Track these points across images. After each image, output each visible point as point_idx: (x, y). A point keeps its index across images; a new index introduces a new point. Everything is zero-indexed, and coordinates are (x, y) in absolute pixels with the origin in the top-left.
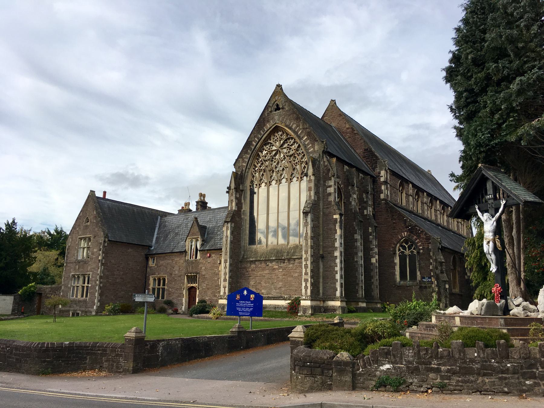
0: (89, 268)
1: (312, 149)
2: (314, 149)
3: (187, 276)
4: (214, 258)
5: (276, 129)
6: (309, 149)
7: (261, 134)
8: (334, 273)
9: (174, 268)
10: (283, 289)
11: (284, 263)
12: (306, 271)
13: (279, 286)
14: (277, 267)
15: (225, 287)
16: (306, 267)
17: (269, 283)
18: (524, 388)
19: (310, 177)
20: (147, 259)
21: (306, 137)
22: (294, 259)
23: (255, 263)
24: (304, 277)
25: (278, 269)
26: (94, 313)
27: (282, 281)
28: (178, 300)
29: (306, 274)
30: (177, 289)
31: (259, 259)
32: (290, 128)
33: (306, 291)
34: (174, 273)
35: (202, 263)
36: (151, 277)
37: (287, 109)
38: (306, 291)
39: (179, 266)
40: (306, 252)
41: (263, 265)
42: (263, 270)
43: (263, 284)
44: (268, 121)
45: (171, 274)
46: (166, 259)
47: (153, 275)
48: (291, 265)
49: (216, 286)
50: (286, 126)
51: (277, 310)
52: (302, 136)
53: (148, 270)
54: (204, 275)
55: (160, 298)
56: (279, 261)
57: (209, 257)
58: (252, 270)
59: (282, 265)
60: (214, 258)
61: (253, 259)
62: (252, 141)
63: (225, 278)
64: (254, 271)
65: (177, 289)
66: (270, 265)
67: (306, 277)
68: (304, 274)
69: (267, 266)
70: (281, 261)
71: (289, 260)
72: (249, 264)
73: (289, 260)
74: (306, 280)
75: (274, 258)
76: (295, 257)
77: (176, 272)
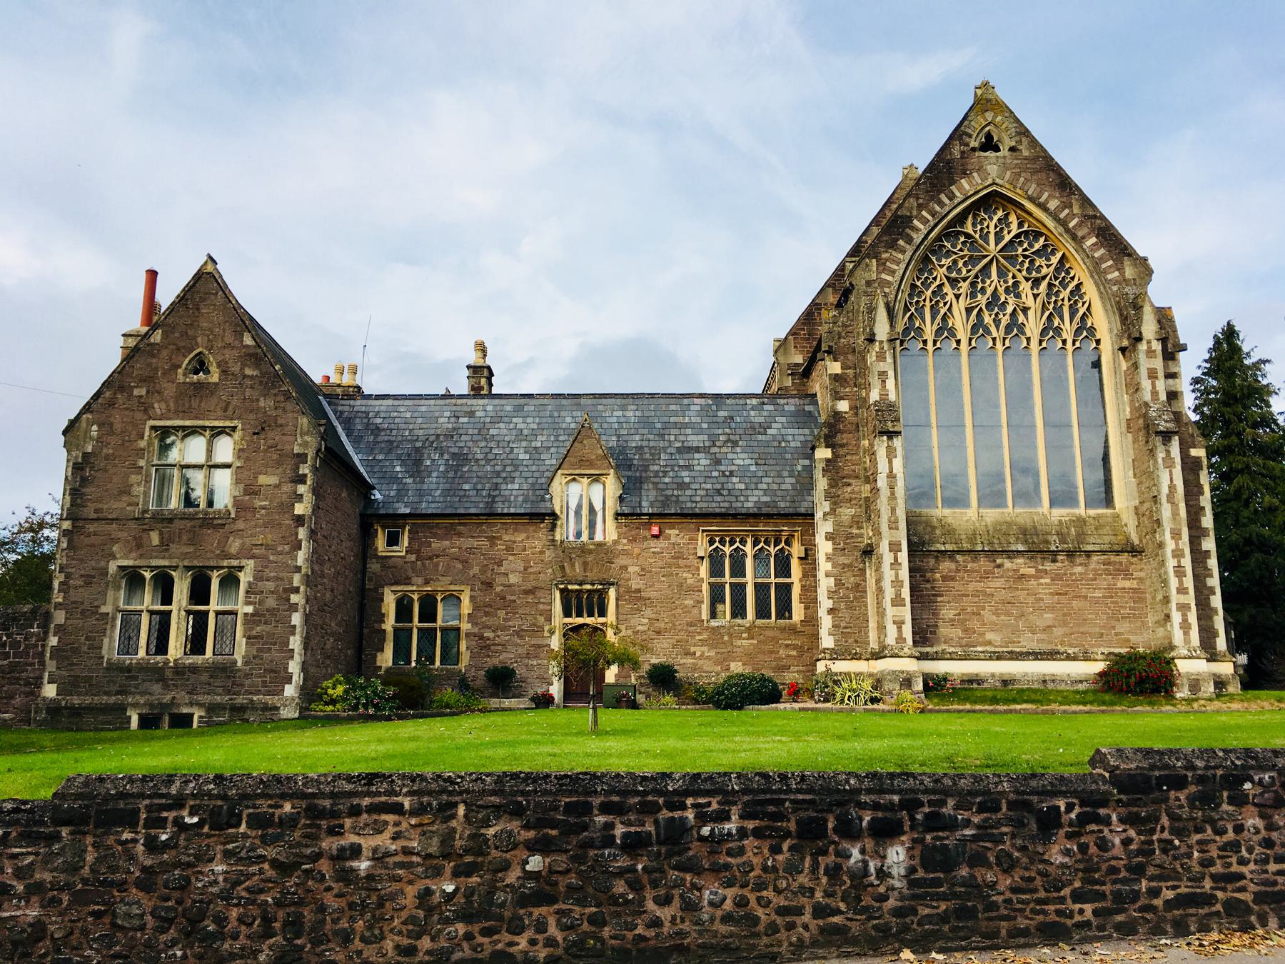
0: (235, 545)
1: (1117, 274)
2: (1122, 274)
3: (562, 591)
4: (673, 540)
5: (990, 201)
6: (1105, 272)
7: (942, 204)
8: (1206, 592)
9: (500, 564)
10: (1058, 632)
11: (1054, 561)
12: (1181, 583)
13: (1041, 624)
14: (1032, 571)
15: (899, 624)
16: (1179, 572)
17: (1008, 614)
18: (968, 832)
19: (1149, 342)
20: (366, 535)
21: (1094, 240)
22: (1089, 554)
23: (952, 558)
24: (1175, 598)
25: (1036, 577)
26: (289, 713)
27: (1051, 609)
28: (530, 669)
29: (1182, 590)
30: (519, 633)
31: (966, 546)
32: (1043, 207)
33: (1186, 634)
34: (500, 580)
35: (626, 553)
36: (387, 591)
37: (1026, 153)
38: (1186, 634)
39: (526, 560)
40: (1176, 535)
41: (983, 564)
42: (985, 577)
43: (987, 615)
44: (965, 173)
45: (489, 585)
46: (460, 535)
47: (397, 583)
48: (1079, 569)
49: (690, 624)
50: (1031, 199)
51: (1050, 686)
52: (1080, 234)
53: (374, 567)
54: (639, 591)
55: (438, 663)
56: (1039, 555)
57: (656, 537)
58: (944, 578)
59: (1048, 566)
60: (673, 540)
61: (949, 547)
62: (910, 219)
63: (898, 595)
64: (953, 579)
65: (519, 633)
66: (1008, 564)
67: (1183, 599)
68: (1174, 591)
69: (999, 566)
70: (1046, 555)
71: (1071, 554)
72: (932, 562)
73: (1071, 554)
74: (1183, 608)
75: (1021, 548)
76: (1090, 548)
77: (513, 579)
